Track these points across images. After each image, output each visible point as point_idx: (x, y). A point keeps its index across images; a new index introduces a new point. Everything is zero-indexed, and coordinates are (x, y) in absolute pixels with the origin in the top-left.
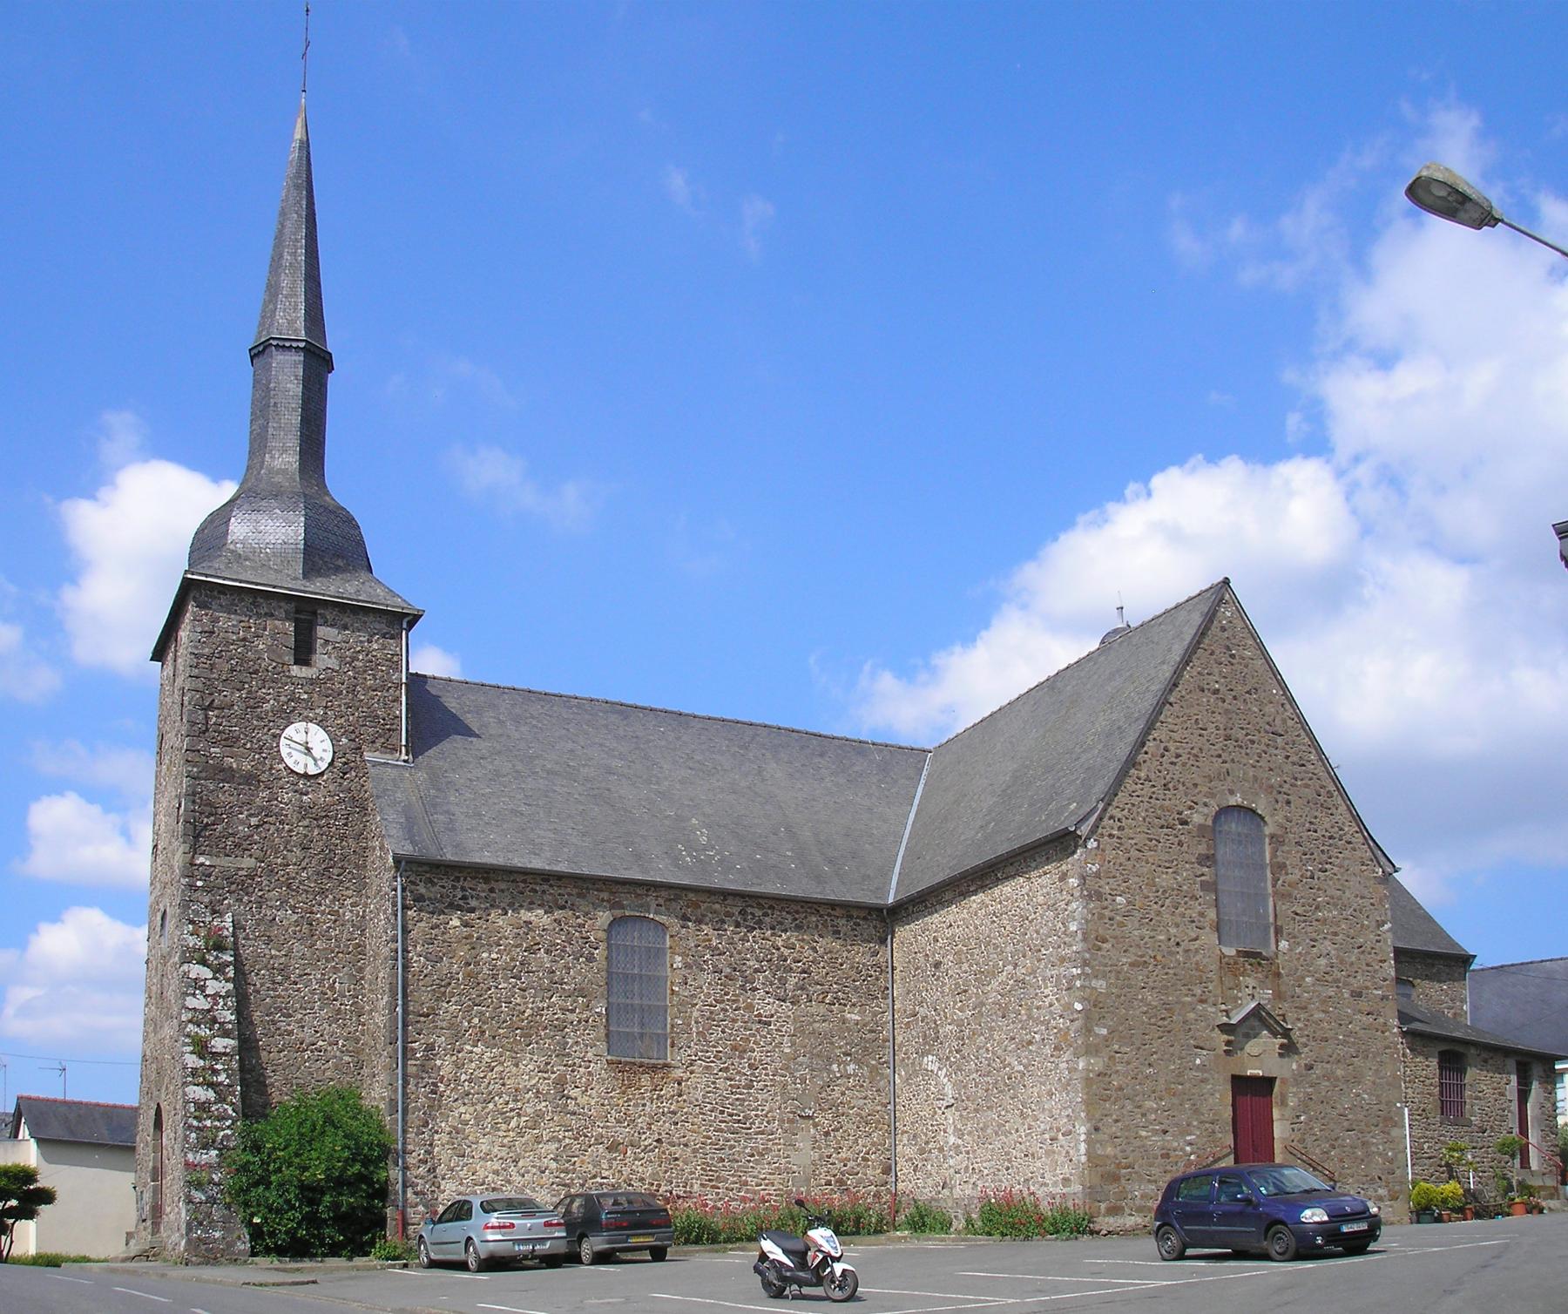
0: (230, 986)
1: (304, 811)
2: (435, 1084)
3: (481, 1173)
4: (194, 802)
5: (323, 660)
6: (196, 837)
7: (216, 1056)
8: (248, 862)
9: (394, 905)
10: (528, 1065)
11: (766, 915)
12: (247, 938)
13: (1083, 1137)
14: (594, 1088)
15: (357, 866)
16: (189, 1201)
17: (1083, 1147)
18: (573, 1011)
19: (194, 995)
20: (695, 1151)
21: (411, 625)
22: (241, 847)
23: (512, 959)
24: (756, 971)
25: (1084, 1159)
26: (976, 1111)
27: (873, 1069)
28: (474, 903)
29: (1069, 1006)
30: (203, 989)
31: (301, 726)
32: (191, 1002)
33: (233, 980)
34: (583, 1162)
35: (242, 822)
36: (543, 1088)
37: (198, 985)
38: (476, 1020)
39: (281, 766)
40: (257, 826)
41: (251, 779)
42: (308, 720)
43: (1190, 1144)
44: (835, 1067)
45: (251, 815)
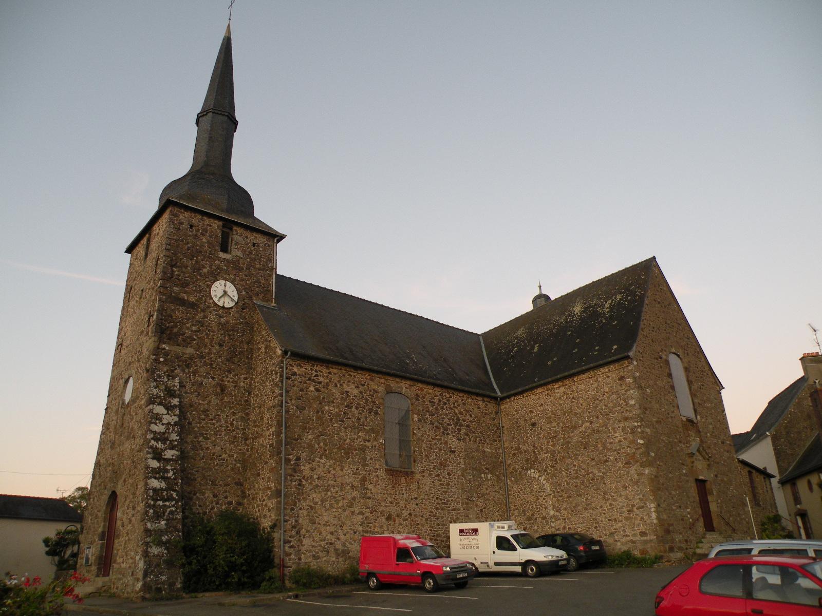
0: (176, 419)
1: (222, 326)
2: (300, 480)
3: (324, 533)
4: (162, 314)
5: (236, 252)
6: (162, 333)
7: (167, 461)
8: (190, 351)
9: (281, 376)
10: (348, 470)
11: (451, 397)
12: (186, 393)
13: (653, 510)
14: (379, 486)
15: (247, 358)
16: (146, 554)
17: (654, 515)
18: (369, 441)
19: (156, 424)
20: (427, 520)
21: (278, 241)
22: (186, 343)
23: (340, 411)
24: (448, 424)
25: (655, 521)
26: (569, 497)
27: (498, 477)
28: (321, 379)
29: (634, 442)
30: (160, 420)
31: (223, 282)
32: (154, 427)
33: (179, 416)
34: (375, 527)
35: (188, 328)
36: (355, 484)
37: (158, 418)
38: (322, 444)
39: (211, 301)
40: (195, 331)
41: (193, 305)
42: (225, 279)
43: (689, 514)
44: (483, 475)
45: (193, 325)
